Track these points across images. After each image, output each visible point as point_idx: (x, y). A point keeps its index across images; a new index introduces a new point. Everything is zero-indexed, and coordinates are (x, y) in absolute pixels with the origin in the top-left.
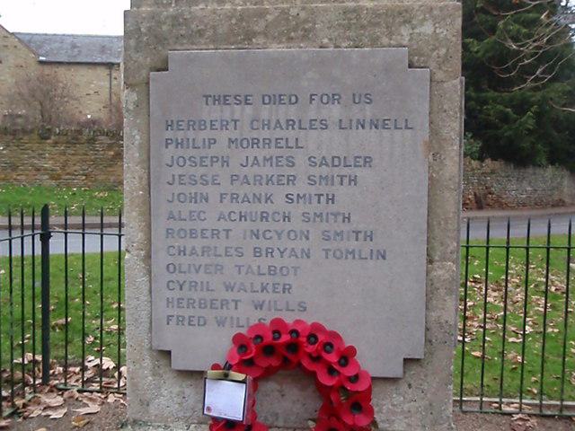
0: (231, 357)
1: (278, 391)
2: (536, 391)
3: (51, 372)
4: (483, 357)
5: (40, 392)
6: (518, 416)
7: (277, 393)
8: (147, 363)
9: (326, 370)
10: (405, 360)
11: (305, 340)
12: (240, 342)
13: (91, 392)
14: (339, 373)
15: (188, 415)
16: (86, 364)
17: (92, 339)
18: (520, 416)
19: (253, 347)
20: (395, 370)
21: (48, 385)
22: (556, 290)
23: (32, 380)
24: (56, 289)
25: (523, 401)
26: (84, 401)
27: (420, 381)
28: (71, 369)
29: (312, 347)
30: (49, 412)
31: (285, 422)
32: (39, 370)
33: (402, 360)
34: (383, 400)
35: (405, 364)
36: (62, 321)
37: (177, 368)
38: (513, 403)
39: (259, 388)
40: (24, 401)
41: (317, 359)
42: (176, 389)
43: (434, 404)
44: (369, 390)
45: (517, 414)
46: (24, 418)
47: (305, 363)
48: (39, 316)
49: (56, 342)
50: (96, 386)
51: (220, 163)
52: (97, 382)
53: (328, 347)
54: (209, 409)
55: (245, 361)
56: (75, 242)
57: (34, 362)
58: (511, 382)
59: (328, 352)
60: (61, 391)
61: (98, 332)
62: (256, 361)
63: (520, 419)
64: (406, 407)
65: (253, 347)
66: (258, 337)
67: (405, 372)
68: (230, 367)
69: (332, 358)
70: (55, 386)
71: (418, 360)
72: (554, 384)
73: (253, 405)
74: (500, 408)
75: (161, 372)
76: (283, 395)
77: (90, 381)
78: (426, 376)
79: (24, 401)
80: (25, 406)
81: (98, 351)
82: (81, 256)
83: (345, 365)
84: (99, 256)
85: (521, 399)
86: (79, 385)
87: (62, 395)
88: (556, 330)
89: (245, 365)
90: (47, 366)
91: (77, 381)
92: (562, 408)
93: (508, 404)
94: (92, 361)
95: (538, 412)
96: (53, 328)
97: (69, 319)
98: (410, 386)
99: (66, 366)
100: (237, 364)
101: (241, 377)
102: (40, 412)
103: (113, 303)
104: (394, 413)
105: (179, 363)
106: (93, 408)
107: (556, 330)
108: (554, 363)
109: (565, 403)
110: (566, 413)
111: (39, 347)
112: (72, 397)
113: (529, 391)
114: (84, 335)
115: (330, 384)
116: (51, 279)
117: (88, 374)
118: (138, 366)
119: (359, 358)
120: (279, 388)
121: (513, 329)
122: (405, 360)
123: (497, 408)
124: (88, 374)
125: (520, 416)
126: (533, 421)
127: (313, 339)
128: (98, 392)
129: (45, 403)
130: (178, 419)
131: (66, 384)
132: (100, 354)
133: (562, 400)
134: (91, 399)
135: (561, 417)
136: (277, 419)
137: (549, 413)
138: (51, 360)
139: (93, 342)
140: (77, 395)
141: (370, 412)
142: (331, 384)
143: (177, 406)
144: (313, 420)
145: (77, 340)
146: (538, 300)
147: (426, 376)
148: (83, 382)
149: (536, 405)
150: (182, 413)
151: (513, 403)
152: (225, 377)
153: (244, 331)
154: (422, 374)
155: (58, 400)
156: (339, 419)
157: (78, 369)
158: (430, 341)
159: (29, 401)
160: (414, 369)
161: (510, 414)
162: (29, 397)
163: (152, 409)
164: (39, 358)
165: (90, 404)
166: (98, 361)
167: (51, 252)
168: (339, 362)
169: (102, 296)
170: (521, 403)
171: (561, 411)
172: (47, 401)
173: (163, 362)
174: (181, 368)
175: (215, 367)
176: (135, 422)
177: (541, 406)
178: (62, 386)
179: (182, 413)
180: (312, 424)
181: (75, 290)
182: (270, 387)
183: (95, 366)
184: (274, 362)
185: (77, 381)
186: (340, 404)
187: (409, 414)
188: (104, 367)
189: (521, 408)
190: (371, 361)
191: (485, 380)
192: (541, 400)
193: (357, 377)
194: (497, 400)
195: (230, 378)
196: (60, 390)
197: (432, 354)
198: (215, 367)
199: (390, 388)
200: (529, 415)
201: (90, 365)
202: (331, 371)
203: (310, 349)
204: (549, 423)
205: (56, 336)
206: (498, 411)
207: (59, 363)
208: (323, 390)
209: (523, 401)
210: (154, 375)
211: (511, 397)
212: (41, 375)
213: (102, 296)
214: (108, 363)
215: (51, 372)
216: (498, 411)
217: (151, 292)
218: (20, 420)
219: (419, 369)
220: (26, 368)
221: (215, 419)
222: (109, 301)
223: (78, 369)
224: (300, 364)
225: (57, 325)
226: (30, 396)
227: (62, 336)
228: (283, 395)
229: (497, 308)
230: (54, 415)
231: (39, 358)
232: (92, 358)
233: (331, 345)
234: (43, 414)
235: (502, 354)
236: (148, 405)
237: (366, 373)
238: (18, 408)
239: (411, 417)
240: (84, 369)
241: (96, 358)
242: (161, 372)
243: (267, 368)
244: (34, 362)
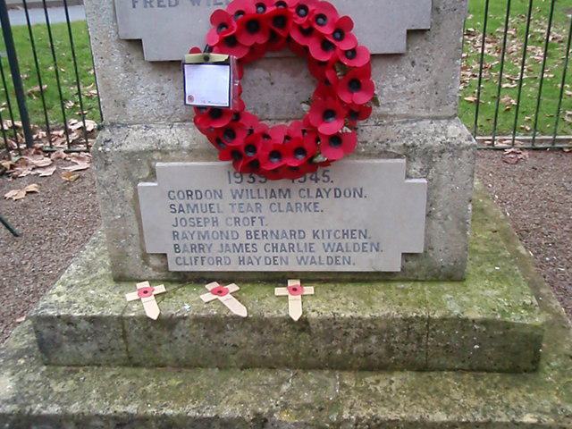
0: (209, 36)
1: (267, 79)
2: (529, 129)
3: (35, 136)
4: (477, 102)
5: (27, 154)
6: (510, 150)
7: (266, 81)
8: (117, 57)
9: (319, 46)
10: (409, 32)
11: (294, 10)
12: (219, 20)
13: (79, 152)
14: (334, 47)
15: (169, 112)
16: (70, 127)
17: (72, 104)
18: (512, 149)
19: (234, 24)
20: (398, 45)
21: (33, 148)
22: (553, 39)
23: (15, 145)
24: (24, 59)
25: (516, 137)
26: (73, 160)
27: (426, 58)
28: (55, 133)
29: (300, 19)
30: (39, 171)
31: (276, 113)
32: (21, 135)
33: (405, 33)
34: (383, 81)
35: (408, 38)
36: (38, 88)
37: (149, 59)
38: (505, 140)
39: (245, 76)
40: (10, 162)
41: (308, 32)
42: (154, 85)
43: (440, 82)
44: (368, 64)
45: (510, 148)
46: (14, 178)
47: (296, 37)
48: (11, 85)
49: (35, 109)
50: (82, 147)
51: (211, 223)
52: (82, 143)
53: (320, 20)
54: (191, 98)
55: (226, 39)
56: (37, 17)
57: (14, 127)
58: (505, 122)
59: (322, 25)
60: (48, 153)
61: (77, 97)
62: (241, 41)
63: (513, 152)
64: (409, 87)
65: (234, 24)
66: (239, 12)
67: (408, 48)
68: (210, 49)
69: (327, 30)
70: (40, 149)
71: (423, 31)
72: (547, 122)
73: (239, 95)
74: (493, 144)
75: (134, 66)
76: (272, 84)
77: (75, 142)
78: (431, 51)
79: (10, 162)
80: (12, 167)
81: (80, 114)
82: (46, 26)
83: (340, 40)
84: (67, 26)
85: (514, 135)
86: (65, 146)
87: (49, 156)
88: (551, 76)
89: (227, 43)
90: (28, 133)
91: (63, 143)
92: (554, 141)
93: (501, 141)
94: (74, 124)
95: (529, 146)
96: (29, 95)
97: (45, 86)
98: (413, 63)
99: (48, 131)
100: (218, 45)
101: (223, 57)
102: (29, 172)
103: (90, 70)
104: (395, 95)
105: (153, 52)
106: (82, 165)
107: (551, 76)
108: (547, 104)
109: (557, 137)
110: (557, 145)
111: (16, 111)
112: (59, 158)
113: (522, 128)
114: (63, 101)
115: (324, 59)
116: (17, 50)
117: (73, 137)
118: (107, 62)
119: (357, 31)
120: (267, 75)
121: (507, 76)
122: (409, 32)
123: (489, 145)
124: (73, 137)
125: (512, 149)
126: (526, 154)
127: (302, 12)
128: (85, 152)
129: (33, 164)
130: (160, 117)
131: (51, 146)
132: (82, 117)
133: (555, 134)
134: (79, 158)
135: (552, 150)
136: (268, 110)
137: (541, 146)
138: (32, 125)
139: (73, 106)
140: (65, 155)
141: (370, 89)
142: (325, 60)
143: (156, 104)
144: (307, 103)
145: (57, 106)
146: (533, 49)
147: (431, 51)
148: (69, 145)
149: (528, 141)
150: (162, 111)
151: (505, 140)
152: (206, 60)
153: (224, 7)
154: (427, 48)
155: (47, 161)
156: (335, 96)
157: (61, 132)
158: (438, 9)
159: (16, 162)
160: (419, 43)
161: (503, 149)
162: (15, 159)
163: (130, 110)
164: (19, 124)
165: (78, 162)
166: (81, 124)
167: (15, 41)
168: (333, 34)
169: (75, 63)
170: (514, 139)
171: (553, 144)
172: (35, 162)
173: (134, 55)
174: (152, 60)
175: (195, 50)
176: (112, 124)
177: (533, 141)
178: (47, 149)
179: (162, 111)
180: (305, 107)
181: (45, 59)
182: (256, 74)
183: (78, 129)
184: (261, 39)
185: (63, 143)
186: (337, 81)
187: (412, 96)
188: (89, 129)
189: (513, 144)
190: (370, 35)
191: (478, 121)
192: (534, 136)
193: (354, 51)
194: (491, 138)
195: (211, 60)
196: (47, 152)
197: (438, 24)
198: (195, 50)
199: (391, 66)
200: (521, 149)
201: (73, 128)
202: (326, 45)
203: (300, 21)
204: (541, 155)
205: (32, 103)
206: (491, 147)
207: (42, 128)
208: (316, 68)
209: (516, 137)
210: (126, 71)
211: (504, 135)
212: (24, 140)
213: (75, 63)
214: (90, 125)
215: (35, 136)
216: (491, 147)
217: (115, 17)
218: (10, 180)
219: (424, 43)
220: (6, 133)
221: (198, 108)
222: (85, 67)
223: (61, 132)
224: (289, 39)
225: (33, 92)
226: (17, 159)
227: (40, 102)
228: (272, 84)
229: (492, 59)
230: (43, 173)
231: (19, 124)
232: (75, 121)
233: (324, 17)
234: (33, 173)
235: (497, 98)
236: (124, 105)
237: (364, 49)
238: (6, 169)
239: (414, 98)
240: (68, 132)
241: (79, 121)
242: (134, 66)
243: (252, 48)
244: (14, 127)
